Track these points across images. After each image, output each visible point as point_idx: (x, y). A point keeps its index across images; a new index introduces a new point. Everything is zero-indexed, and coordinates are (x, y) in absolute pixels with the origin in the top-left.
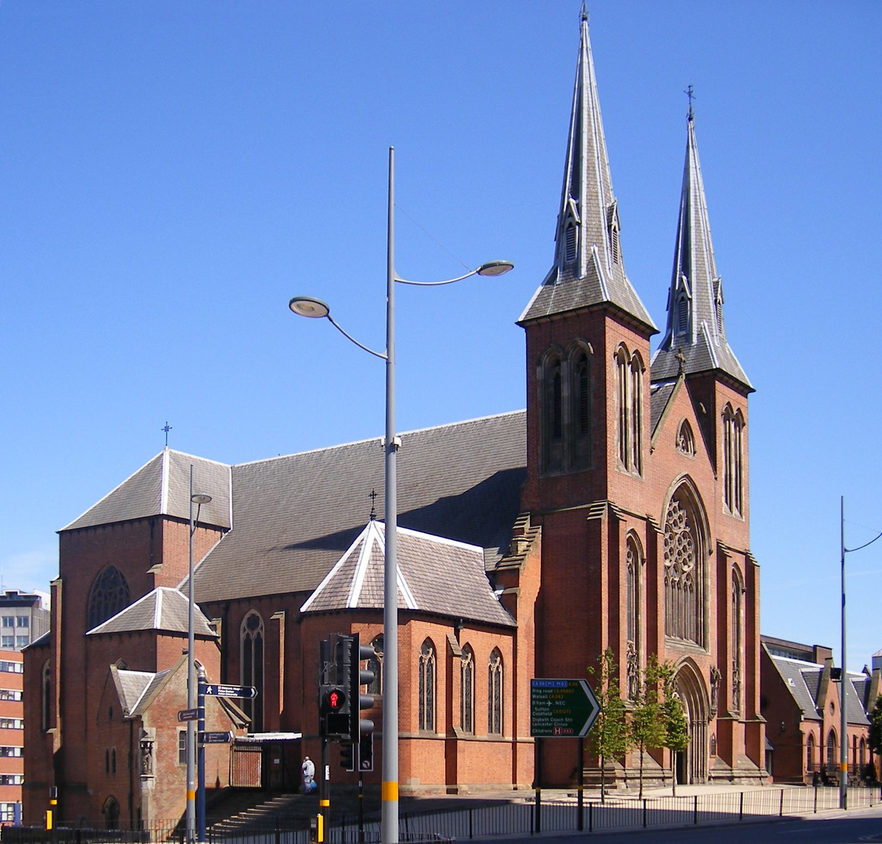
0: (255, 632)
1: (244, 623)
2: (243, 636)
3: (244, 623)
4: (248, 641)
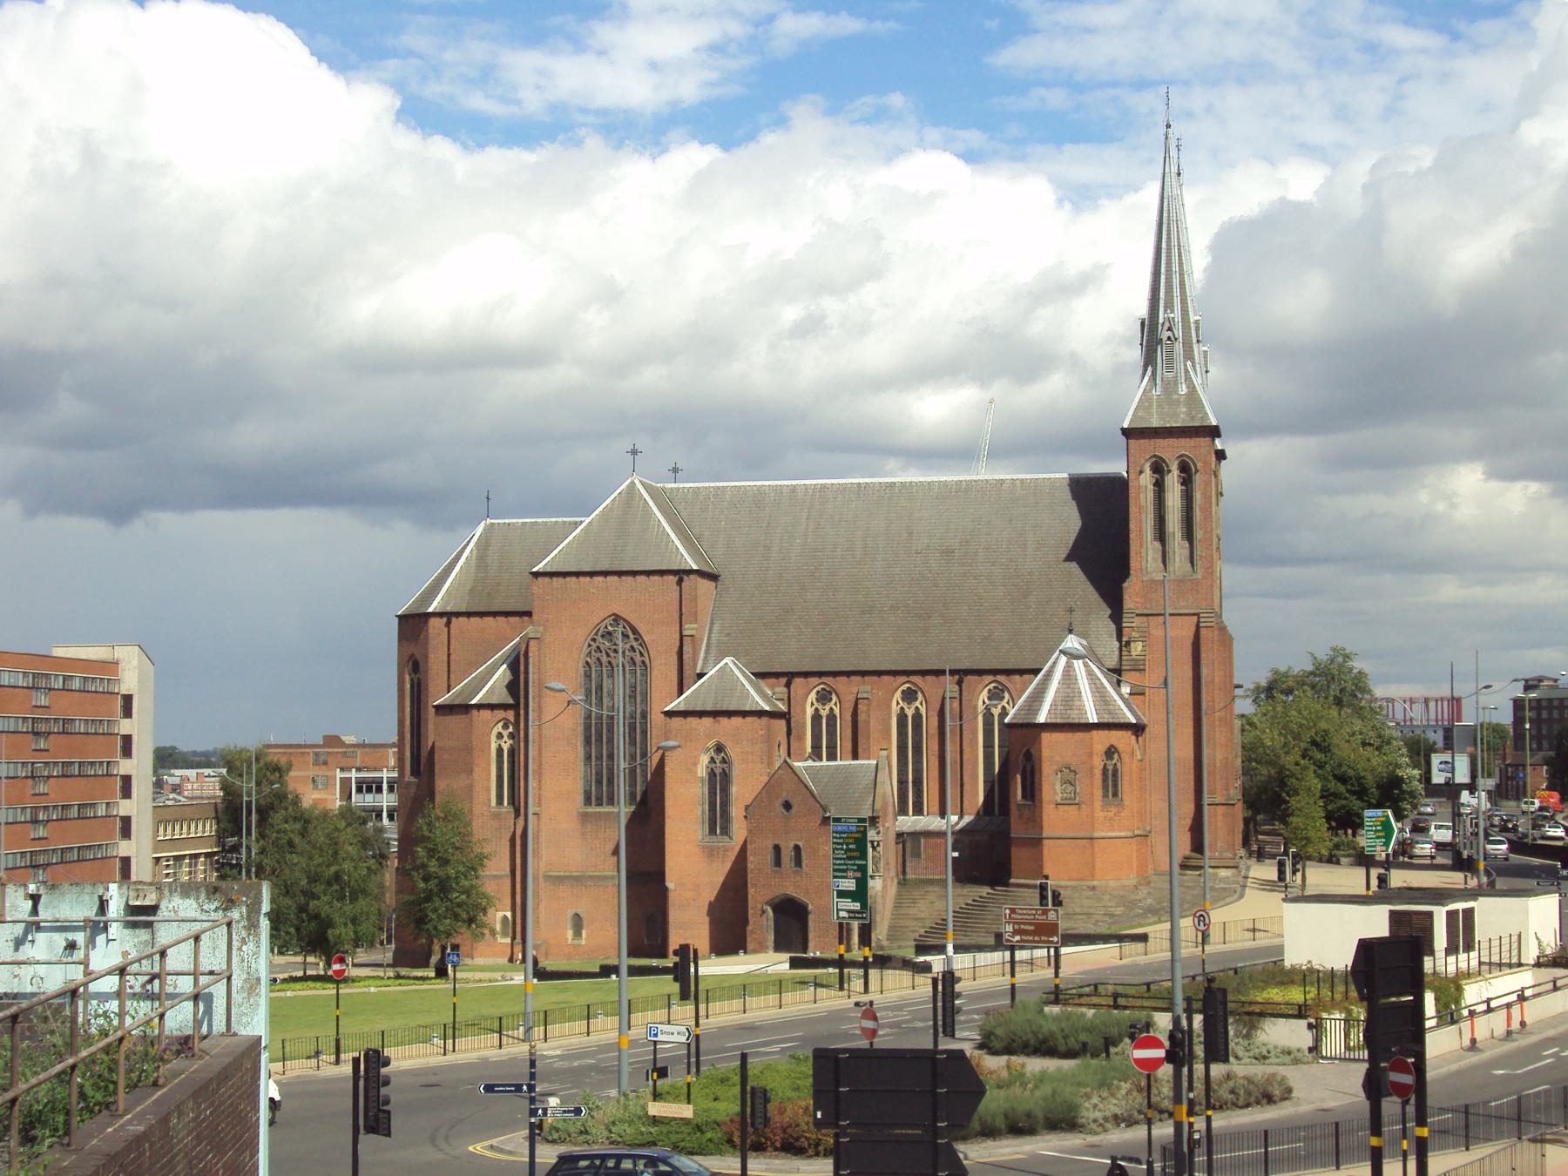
0: (827, 708)
3: (898, 695)
4: (816, 717)
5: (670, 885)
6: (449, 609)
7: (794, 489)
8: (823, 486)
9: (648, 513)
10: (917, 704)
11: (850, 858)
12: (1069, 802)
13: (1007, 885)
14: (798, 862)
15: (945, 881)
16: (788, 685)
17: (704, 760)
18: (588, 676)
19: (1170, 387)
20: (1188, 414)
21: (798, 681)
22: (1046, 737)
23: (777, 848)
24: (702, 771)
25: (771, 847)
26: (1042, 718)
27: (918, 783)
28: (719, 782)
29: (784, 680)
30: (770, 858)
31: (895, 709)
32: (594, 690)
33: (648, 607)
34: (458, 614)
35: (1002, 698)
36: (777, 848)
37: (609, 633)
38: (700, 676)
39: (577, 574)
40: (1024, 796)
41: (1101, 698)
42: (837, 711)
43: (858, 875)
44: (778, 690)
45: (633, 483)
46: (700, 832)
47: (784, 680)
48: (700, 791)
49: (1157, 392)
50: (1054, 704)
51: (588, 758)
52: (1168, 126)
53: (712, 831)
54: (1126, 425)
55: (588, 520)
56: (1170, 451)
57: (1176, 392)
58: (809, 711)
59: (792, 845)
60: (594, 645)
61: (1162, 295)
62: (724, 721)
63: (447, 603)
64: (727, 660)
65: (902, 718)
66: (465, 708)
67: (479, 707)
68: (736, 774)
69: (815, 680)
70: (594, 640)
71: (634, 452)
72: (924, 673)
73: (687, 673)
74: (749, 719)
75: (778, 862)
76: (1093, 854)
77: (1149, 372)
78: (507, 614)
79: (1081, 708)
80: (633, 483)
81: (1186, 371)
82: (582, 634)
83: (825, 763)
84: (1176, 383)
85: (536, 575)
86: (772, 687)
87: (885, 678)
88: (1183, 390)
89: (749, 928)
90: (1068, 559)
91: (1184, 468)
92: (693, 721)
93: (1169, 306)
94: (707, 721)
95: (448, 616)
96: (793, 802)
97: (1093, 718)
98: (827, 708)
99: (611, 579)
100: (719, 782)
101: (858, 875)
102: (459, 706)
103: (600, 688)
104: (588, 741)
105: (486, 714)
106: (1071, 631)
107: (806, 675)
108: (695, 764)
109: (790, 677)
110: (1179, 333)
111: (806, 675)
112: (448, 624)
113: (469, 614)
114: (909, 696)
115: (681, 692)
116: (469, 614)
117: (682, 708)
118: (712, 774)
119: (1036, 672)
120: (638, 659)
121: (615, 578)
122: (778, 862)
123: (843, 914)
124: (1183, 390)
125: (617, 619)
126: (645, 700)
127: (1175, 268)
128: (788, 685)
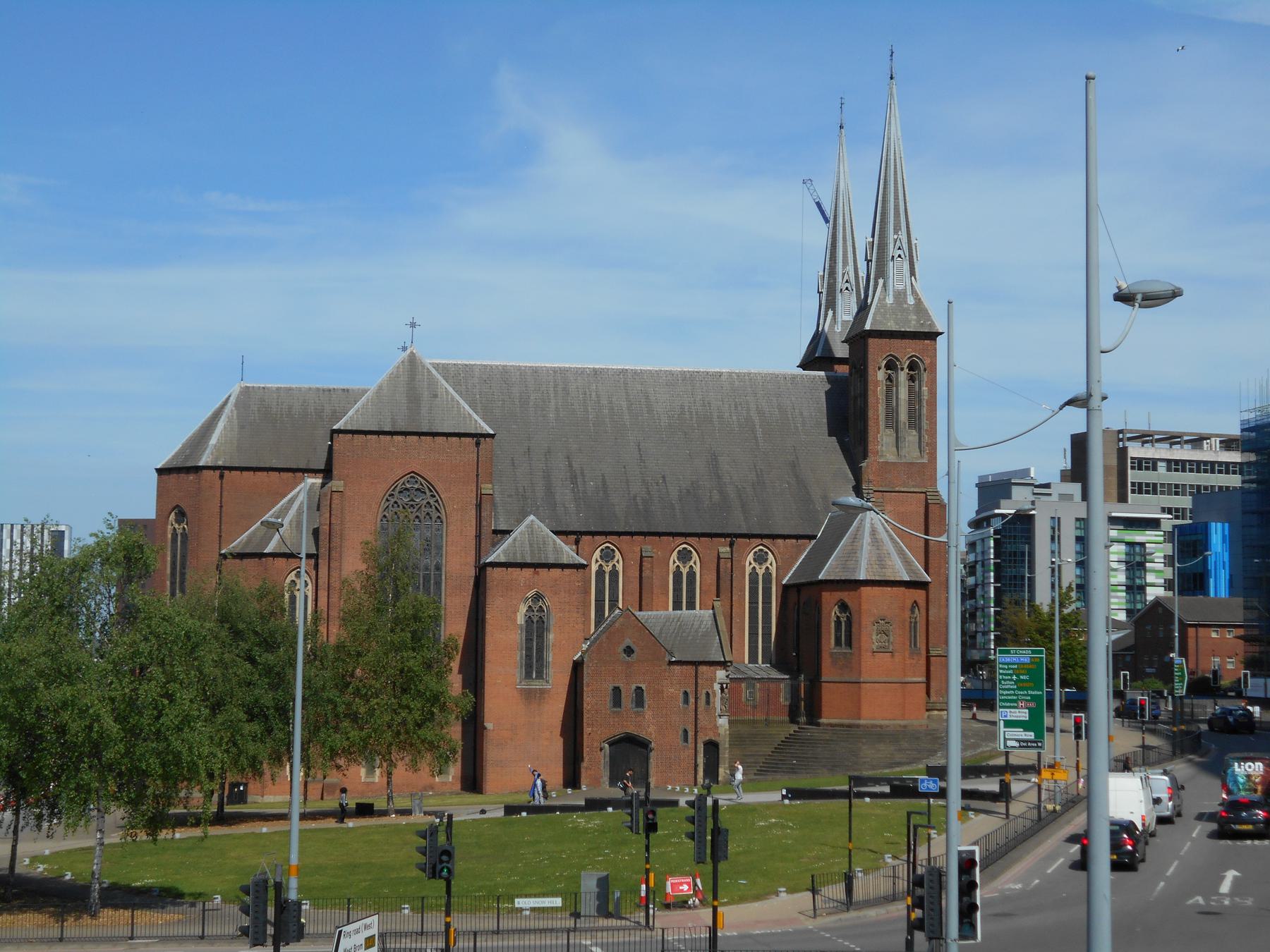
0: (611, 565)
1: (675, 554)
2: (672, 568)
3: (675, 554)
5: (489, 725)
6: (220, 463)
10: (692, 563)
11: (1019, 689)
12: (882, 650)
13: (818, 725)
14: (639, 702)
17: (523, 609)
20: (918, 321)
22: (865, 590)
23: (617, 691)
24: (521, 619)
25: (611, 688)
28: (536, 629)
30: (609, 699)
31: (672, 568)
33: (445, 468)
34: (231, 469)
35: (766, 560)
36: (617, 691)
40: (838, 642)
42: (620, 567)
43: (1032, 705)
46: (518, 675)
48: (517, 637)
53: (528, 675)
57: (906, 302)
59: (634, 687)
60: (393, 500)
62: (543, 572)
63: (217, 459)
64: (532, 517)
65: (678, 575)
67: (273, 555)
68: (553, 621)
71: (413, 325)
74: (567, 571)
75: (617, 702)
82: (381, 489)
83: (684, 611)
87: (664, 538)
89: (584, 765)
92: (516, 572)
94: (528, 572)
96: (634, 647)
98: (611, 565)
100: (536, 629)
101: (1032, 705)
105: (281, 562)
108: (515, 612)
112: (222, 477)
117: (503, 559)
118: (529, 621)
120: (434, 515)
122: (617, 702)
123: (1010, 743)
124: (911, 300)
125: (414, 474)
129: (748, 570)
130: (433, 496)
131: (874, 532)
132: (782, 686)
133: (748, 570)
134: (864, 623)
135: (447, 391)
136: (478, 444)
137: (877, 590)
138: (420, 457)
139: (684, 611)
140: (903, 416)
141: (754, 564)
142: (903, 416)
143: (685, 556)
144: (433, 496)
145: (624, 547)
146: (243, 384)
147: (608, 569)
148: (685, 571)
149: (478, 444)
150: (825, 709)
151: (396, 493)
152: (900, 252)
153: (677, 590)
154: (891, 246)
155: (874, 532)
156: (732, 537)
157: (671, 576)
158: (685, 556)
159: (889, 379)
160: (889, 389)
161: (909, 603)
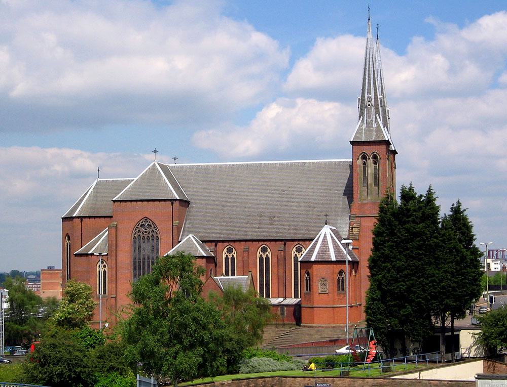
1: (260, 249)
3: (260, 249)
4: (227, 258)
7: (221, 166)
8: (233, 165)
9: (160, 176)
10: (267, 253)
15: (100, 323)
16: (216, 245)
18: (135, 242)
19: (369, 124)
21: (220, 244)
22: (315, 266)
26: (313, 259)
27: (268, 285)
29: (214, 244)
31: (258, 255)
32: (137, 248)
34: (85, 217)
37: (143, 225)
38: (180, 241)
39: (131, 201)
40: (307, 290)
41: (337, 251)
42: (235, 256)
44: (211, 248)
45: (154, 164)
47: (214, 244)
49: (364, 126)
50: (318, 253)
51: (135, 275)
52: (369, 19)
54: (352, 141)
55: (135, 179)
56: (368, 150)
58: (224, 256)
60: (138, 230)
61: (366, 88)
63: (81, 213)
64: (190, 236)
65: (261, 259)
66: (87, 255)
69: (226, 244)
70: (137, 227)
72: (234, 241)
73: (175, 241)
76: (334, 313)
77: (362, 117)
78: (105, 217)
79: (329, 255)
80: (154, 164)
81: (376, 118)
83: (230, 277)
84: (372, 124)
85: (115, 201)
86: (209, 247)
88: (375, 126)
90: (430, 193)
91: (375, 157)
93: (369, 92)
95: (81, 218)
97: (333, 259)
98: (231, 255)
99: (156, 203)
102: (84, 254)
103: (140, 247)
104: (135, 269)
106: (326, 224)
107: (223, 241)
109: (216, 242)
110: (373, 102)
111: (223, 241)
113: (90, 217)
114: (230, 251)
115: (173, 248)
116: (90, 217)
119: (313, 240)
121: (146, 203)
124: (375, 126)
125: (146, 219)
126: (158, 252)
127: (372, 76)
128: (216, 245)
129: (293, 255)
130: (154, 227)
131: (325, 241)
132: (279, 308)
133: (293, 255)
134: (314, 280)
135: (165, 180)
136: (172, 203)
137: (320, 266)
138: (148, 210)
139: (230, 277)
140: (370, 180)
141: (296, 253)
142: (370, 180)
143: (264, 250)
144: (154, 227)
145: (237, 247)
146: (99, 180)
147: (230, 257)
148: (264, 257)
149: (172, 203)
150: (302, 321)
151: (139, 226)
152: (369, 103)
153: (227, 266)
154: (366, 100)
155: (325, 241)
156: (285, 241)
157: (258, 259)
158: (264, 250)
159: (364, 164)
160: (364, 168)
161: (338, 271)
